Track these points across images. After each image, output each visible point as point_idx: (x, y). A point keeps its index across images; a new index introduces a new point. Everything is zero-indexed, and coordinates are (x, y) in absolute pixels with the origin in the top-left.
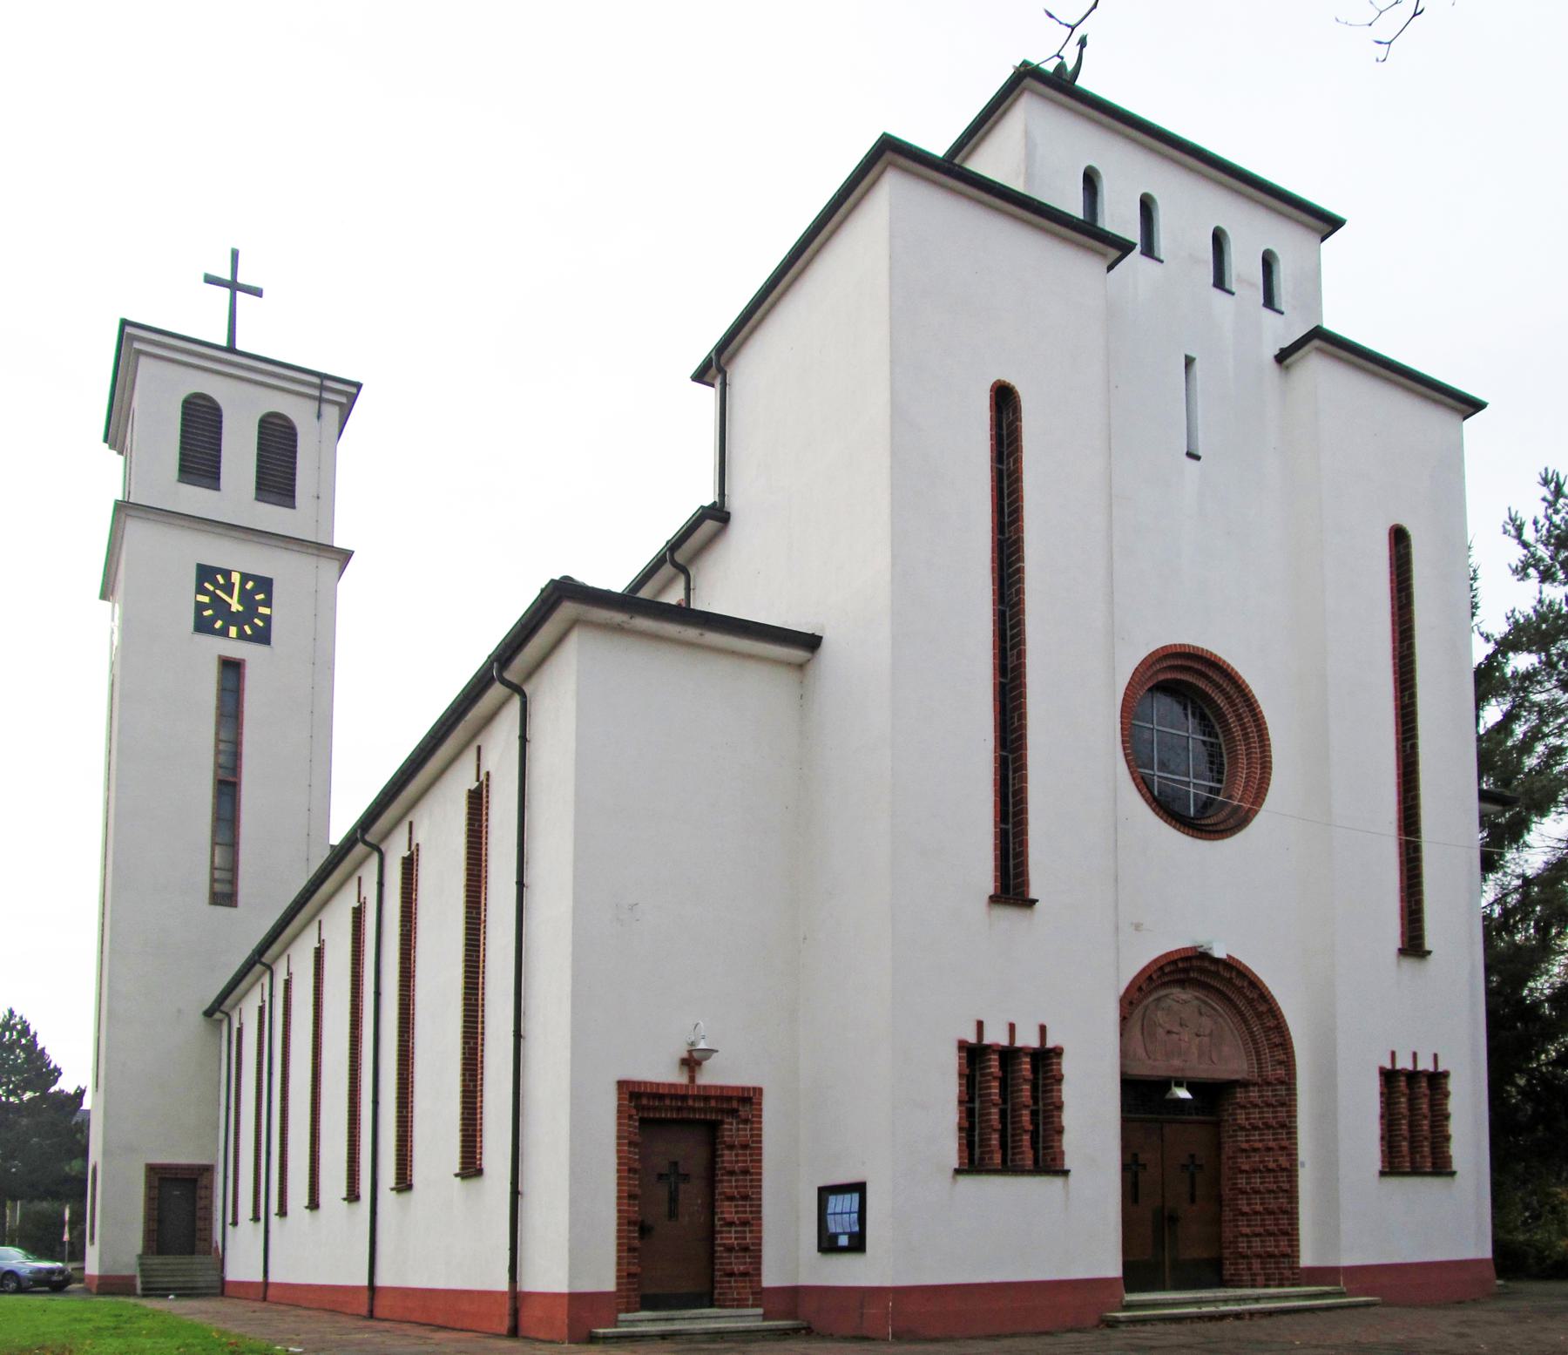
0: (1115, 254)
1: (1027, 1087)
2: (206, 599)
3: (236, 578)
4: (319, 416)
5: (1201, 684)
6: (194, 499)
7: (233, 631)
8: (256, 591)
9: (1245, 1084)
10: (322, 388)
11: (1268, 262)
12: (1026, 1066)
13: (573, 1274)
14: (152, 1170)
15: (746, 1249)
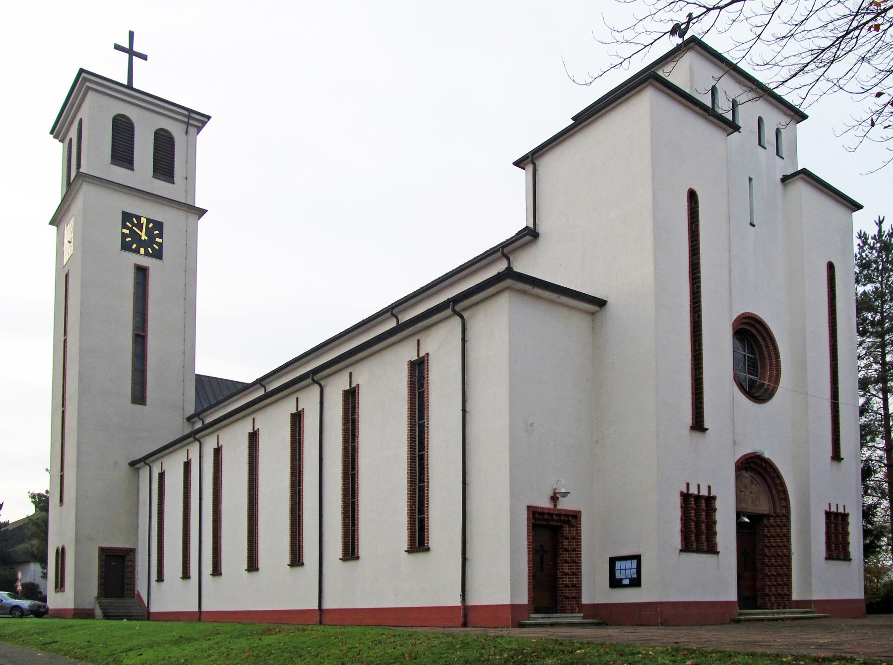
0: (731, 130)
1: (704, 513)
2: (127, 232)
3: (143, 220)
4: (187, 133)
5: (753, 331)
6: (119, 174)
7: (142, 251)
8: (154, 229)
9: (768, 516)
10: (189, 117)
11: (778, 132)
12: (703, 504)
13: (512, 595)
14: (102, 550)
15: (574, 586)
